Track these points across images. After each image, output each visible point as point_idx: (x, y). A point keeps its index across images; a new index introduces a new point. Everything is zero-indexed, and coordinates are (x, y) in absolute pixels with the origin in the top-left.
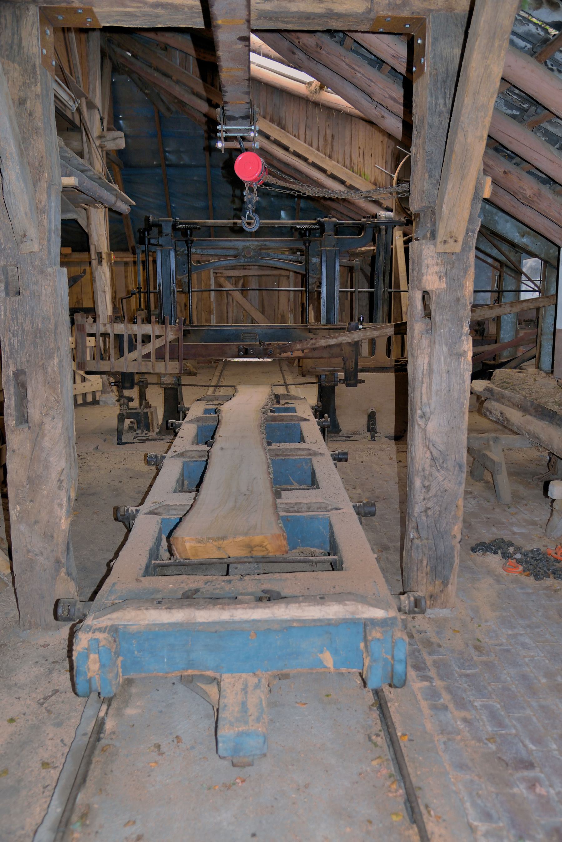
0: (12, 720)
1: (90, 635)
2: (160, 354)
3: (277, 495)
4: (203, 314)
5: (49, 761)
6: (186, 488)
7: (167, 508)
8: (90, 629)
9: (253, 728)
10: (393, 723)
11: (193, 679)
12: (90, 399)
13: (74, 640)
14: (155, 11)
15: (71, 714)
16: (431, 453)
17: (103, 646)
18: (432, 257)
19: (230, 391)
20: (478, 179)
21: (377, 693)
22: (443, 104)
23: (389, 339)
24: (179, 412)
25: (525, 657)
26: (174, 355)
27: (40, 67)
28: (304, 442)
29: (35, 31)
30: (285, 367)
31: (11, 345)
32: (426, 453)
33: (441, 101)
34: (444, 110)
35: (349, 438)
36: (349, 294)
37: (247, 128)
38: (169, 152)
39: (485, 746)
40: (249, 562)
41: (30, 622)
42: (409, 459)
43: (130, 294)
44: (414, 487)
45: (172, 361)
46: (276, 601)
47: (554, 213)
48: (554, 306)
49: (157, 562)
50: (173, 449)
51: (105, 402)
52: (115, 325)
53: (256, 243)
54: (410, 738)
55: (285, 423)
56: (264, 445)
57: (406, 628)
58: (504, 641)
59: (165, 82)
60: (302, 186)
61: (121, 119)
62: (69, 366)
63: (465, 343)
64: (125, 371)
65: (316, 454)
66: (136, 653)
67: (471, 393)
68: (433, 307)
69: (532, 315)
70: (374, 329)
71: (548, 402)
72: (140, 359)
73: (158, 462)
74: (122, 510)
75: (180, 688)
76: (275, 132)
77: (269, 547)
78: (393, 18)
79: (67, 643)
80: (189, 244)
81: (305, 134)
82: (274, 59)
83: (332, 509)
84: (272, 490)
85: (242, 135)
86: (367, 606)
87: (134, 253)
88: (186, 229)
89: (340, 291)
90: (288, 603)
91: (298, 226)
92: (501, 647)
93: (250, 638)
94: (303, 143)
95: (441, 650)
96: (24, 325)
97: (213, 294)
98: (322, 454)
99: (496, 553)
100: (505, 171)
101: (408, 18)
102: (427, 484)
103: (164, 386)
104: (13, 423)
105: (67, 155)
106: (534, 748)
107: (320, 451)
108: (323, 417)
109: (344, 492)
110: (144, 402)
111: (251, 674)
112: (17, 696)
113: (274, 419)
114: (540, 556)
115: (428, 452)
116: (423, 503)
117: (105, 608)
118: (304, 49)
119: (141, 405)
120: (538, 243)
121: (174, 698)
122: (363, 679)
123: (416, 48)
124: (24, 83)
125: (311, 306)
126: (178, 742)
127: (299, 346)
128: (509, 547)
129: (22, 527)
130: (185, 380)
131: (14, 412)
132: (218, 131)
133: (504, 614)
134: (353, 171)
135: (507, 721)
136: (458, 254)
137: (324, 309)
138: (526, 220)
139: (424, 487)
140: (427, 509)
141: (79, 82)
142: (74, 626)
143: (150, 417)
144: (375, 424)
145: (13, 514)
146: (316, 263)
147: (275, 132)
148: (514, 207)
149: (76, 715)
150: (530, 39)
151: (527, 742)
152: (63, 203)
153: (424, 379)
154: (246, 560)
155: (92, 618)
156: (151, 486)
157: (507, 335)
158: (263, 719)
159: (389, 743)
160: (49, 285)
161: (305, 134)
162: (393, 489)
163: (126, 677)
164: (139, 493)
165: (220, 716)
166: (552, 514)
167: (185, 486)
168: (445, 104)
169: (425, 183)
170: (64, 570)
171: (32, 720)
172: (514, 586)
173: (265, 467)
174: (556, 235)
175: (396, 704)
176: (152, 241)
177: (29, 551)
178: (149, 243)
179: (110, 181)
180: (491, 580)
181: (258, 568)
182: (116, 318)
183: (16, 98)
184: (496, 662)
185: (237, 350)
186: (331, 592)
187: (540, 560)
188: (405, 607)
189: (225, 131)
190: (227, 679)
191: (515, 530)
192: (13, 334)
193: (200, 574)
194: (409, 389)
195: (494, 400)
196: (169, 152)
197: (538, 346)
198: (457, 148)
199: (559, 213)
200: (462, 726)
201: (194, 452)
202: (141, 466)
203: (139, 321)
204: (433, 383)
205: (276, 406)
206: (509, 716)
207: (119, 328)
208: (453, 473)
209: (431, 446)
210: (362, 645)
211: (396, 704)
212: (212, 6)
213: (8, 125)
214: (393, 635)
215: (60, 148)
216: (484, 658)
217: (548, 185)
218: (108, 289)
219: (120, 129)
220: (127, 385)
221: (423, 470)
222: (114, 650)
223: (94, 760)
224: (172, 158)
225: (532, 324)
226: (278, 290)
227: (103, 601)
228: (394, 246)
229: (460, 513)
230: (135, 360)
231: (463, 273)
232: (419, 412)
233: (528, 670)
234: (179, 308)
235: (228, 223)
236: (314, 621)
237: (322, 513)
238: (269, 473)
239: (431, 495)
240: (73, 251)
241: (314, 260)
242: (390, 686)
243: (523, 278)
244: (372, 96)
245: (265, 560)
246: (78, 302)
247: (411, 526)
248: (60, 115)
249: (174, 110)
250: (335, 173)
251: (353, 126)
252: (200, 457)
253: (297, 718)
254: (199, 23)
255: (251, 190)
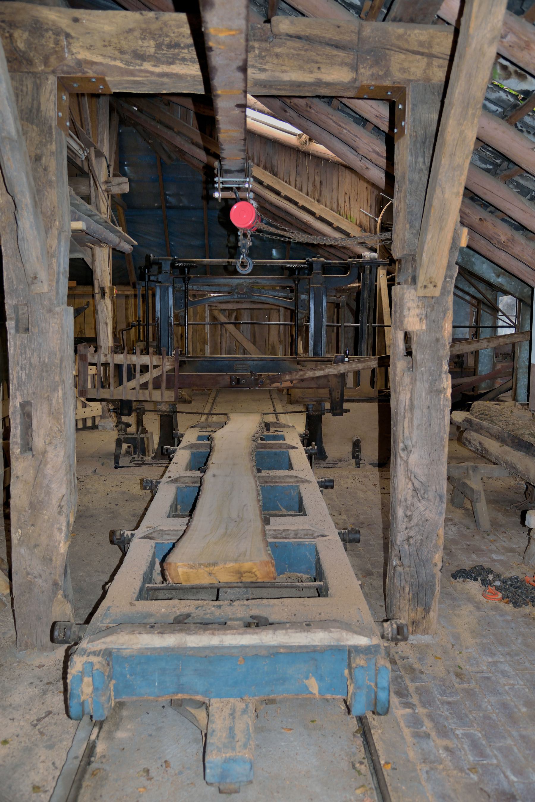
0: (5, 742)
1: (85, 659)
2: (157, 383)
3: (266, 521)
4: (198, 344)
5: (40, 785)
6: (179, 513)
7: (161, 533)
8: (84, 652)
9: (240, 754)
10: (376, 751)
11: (182, 702)
12: (89, 423)
13: (69, 663)
14: (161, 80)
15: (63, 736)
16: (413, 484)
17: (97, 669)
18: (413, 300)
19: (222, 419)
20: (455, 229)
21: (361, 720)
22: (422, 162)
23: (373, 371)
24: (173, 439)
25: (505, 685)
26: (170, 384)
27: (55, 128)
28: (292, 469)
29: (52, 98)
30: (275, 395)
31: (19, 378)
32: (408, 484)
33: (421, 160)
34: (423, 167)
35: (334, 464)
36: (335, 328)
37: (243, 180)
38: (169, 195)
39: (466, 776)
40: (239, 587)
41: (27, 642)
42: (392, 490)
43: (130, 326)
44: (397, 517)
45: (169, 390)
46: (264, 627)
47: (526, 257)
48: (528, 342)
49: (150, 585)
50: (167, 474)
51: (103, 427)
52: (115, 355)
53: (248, 281)
54: (393, 766)
55: (274, 450)
56: (254, 473)
57: (389, 655)
58: (485, 668)
59: (167, 134)
60: (292, 233)
61: (126, 165)
62: (71, 392)
63: (445, 380)
64: (124, 399)
65: (303, 481)
66: (128, 676)
67: (451, 423)
68: (414, 347)
69: (508, 349)
70: (359, 362)
71: (524, 434)
72: (138, 388)
73: (153, 487)
74: (118, 533)
75: (170, 711)
76: (268, 178)
77: (257, 573)
78: (376, 87)
79: (61, 664)
80: (186, 280)
81: (296, 180)
82: (268, 114)
83: (318, 536)
84: (261, 518)
85: (237, 186)
86: (351, 634)
87: (134, 287)
88: (184, 267)
89: (327, 326)
90: (275, 630)
91: (288, 266)
92: (482, 675)
93: (238, 663)
94: (293, 188)
95: (423, 676)
96: (32, 359)
97: (207, 327)
98: (309, 482)
99: (476, 580)
100: (480, 219)
101: (390, 87)
102: (409, 513)
103: (160, 413)
104: (18, 451)
105: (76, 202)
106: (515, 779)
107: (307, 478)
108: (311, 445)
109: (329, 519)
110: (140, 428)
111: (239, 699)
112: (11, 717)
113: (264, 446)
114: (519, 584)
115: (410, 483)
116: (405, 532)
117: (100, 631)
118: (295, 109)
119: (138, 431)
120: (513, 283)
121: (163, 722)
122: (347, 707)
123: (397, 114)
124: (41, 142)
125: (300, 338)
126: (166, 767)
127: (288, 377)
128: (488, 574)
129: (23, 551)
130: (180, 407)
131: (19, 440)
132: (216, 183)
133: (485, 641)
134: (340, 214)
135: (488, 751)
136: (437, 298)
137: (311, 342)
138: (501, 263)
139: (407, 516)
140: (409, 538)
141: (89, 134)
142: (69, 648)
143: (146, 442)
144: (360, 451)
145: (15, 537)
146: (304, 300)
147: (268, 178)
148: (489, 250)
149: (68, 737)
150: (501, 104)
151: (508, 773)
152: (72, 244)
153: (406, 414)
154: (235, 585)
155: (87, 641)
156: (146, 509)
157: (484, 368)
158: (250, 745)
159: (373, 771)
160: (56, 323)
161: (296, 180)
162: (376, 514)
163: (118, 700)
164: (134, 516)
165: (208, 741)
166: (529, 542)
167: (179, 511)
168: (424, 162)
169: (406, 233)
170: (61, 592)
171: (25, 742)
172: (494, 613)
173: (255, 494)
174: (529, 277)
175: (380, 731)
176: (152, 278)
177: (28, 574)
178: (149, 279)
179: (115, 224)
180: (471, 607)
181: (247, 593)
182: (116, 347)
183: (33, 155)
184: (477, 690)
185: (229, 380)
186: (317, 619)
187: (519, 587)
188: (388, 634)
189: (222, 183)
190: (215, 704)
191: (495, 557)
192: (21, 368)
193: (191, 597)
194: (392, 422)
195: (473, 431)
196: (169, 195)
197: (514, 379)
198: (436, 203)
199: (532, 257)
200: (444, 755)
201: (187, 478)
202: (137, 490)
203: (138, 351)
204: (414, 419)
205: (266, 433)
206: (490, 745)
207: (119, 358)
208: (434, 504)
209: (413, 478)
210: (346, 672)
211: (380, 731)
212: (213, 79)
213: (25, 179)
214: (376, 663)
215: (71, 196)
216: (465, 686)
217: (521, 232)
218: (110, 321)
219: (124, 174)
220: (125, 412)
221: (406, 500)
222: (107, 674)
223: (84, 784)
224: (172, 200)
225: (509, 358)
226: (269, 324)
227: (98, 624)
228: (378, 283)
229: (441, 542)
230: (133, 389)
231: (442, 315)
232: (401, 445)
233: (509, 698)
234: (175, 339)
235: (223, 262)
236: (300, 647)
237: (309, 540)
238: (259, 501)
239: (413, 524)
240: (78, 284)
241: (303, 297)
242: (374, 713)
243: (500, 314)
244: (357, 150)
245: (253, 585)
246: (81, 332)
247: (393, 553)
248: (71, 162)
249: (175, 158)
250: (323, 216)
251: (340, 174)
252: (193, 483)
253: (282, 744)
254: (200, 90)
255: (245, 235)
